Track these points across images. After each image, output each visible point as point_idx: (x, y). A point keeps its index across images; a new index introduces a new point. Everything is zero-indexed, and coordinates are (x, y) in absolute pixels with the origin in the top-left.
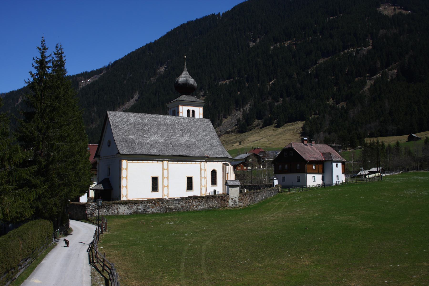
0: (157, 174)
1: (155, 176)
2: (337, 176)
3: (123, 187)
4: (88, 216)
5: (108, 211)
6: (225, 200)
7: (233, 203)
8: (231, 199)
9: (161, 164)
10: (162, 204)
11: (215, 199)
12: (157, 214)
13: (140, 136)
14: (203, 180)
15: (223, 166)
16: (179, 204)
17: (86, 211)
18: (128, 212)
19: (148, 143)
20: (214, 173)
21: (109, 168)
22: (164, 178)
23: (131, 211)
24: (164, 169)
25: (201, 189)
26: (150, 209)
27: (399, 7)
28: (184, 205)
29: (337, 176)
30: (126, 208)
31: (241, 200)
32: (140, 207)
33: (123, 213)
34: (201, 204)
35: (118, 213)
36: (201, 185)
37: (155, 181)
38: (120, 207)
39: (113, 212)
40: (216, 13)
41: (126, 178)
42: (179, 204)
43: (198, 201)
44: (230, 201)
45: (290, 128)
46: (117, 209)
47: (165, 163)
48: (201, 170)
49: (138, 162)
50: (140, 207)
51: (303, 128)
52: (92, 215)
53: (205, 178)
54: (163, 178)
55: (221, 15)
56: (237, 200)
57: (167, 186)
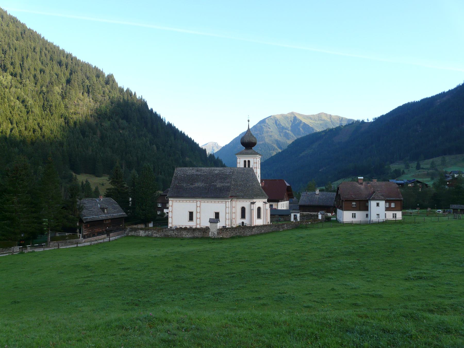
0: (193, 210)
1: (191, 211)
23: (145, 234)
25: (226, 221)
34: (189, 234)
36: (226, 219)
37: (191, 214)
44: (210, 233)
54: (197, 212)
56: (216, 233)
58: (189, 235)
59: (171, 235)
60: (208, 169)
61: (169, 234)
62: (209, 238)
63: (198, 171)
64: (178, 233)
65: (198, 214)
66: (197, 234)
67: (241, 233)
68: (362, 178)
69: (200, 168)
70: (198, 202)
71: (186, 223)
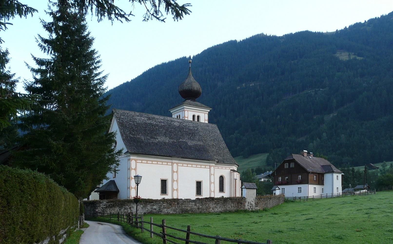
0: (167, 176)
1: (164, 178)
2: (337, 188)
6: (241, 203)
7: (249, 207)
8: (247, 202)
10: (178, 204)
11: (232, 202)
12: (172, 214)
13: (148, 136)
14: (212, 185)
16: (195, 205)
18: (142, 211)
19: (157, 144)
20: (222, 179)
22: (174, 181)
23: (145, 211)
24: (174, 172)
26: (165, 210)
27: (353, 53)
28: (201, 207)
29: (337, 188)
31: (257, 204)
32: (155, 207)
37: (164, 183)
40: (188, 56)
42: (195, 205)
43: (214, 202)
44: (246, 204)
45: (254, 159)
46: (130, 208)
48: (210, 175)
50: (155, 207)
51: (268, 158)
53: (214, 183)
54: (173, 181)
55: (192, 58)
56: (253, 204)
57: (177, 190)
58: (219, 209)
59: (191, 210)
60: (162, 118)
61: (189, 208)
62: (246, 211)
63: (149, 119)
64: (202, 205)
65: (175, 183)
66: (230, 206)
67: (202, 206)
68: (306, 151)
69: (151, 116)
70: (175, 165)
71: (157, 195)
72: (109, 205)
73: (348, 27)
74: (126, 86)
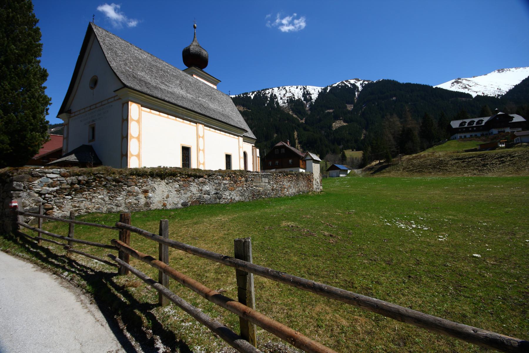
1: (186, 145)
3: (132, 155)
4: (21, 219)
5: (111, 198)
9: (195, 128)
15: (253, 149)
17: (11, 198)
18: (176, 200)
21: (93, 129)
23: (185, 197)
24: (200, 137)
26: (227, 193)
30: (173, 190)
32: (206, 188)
33: (164, 205)
35: (147, 204)
38: (156, 186)
39: (132, 200)
41: (138, 138)
46: (145, 192)
47: (201, 126)
49: (159, 115)
50: (206, 188)
52: (42, 213)
54: (198, 150)
72: (72, 184)
73: (162, 167)
74: (125, 120)
